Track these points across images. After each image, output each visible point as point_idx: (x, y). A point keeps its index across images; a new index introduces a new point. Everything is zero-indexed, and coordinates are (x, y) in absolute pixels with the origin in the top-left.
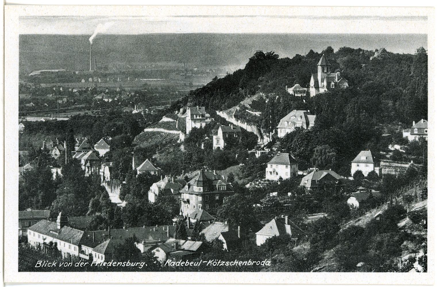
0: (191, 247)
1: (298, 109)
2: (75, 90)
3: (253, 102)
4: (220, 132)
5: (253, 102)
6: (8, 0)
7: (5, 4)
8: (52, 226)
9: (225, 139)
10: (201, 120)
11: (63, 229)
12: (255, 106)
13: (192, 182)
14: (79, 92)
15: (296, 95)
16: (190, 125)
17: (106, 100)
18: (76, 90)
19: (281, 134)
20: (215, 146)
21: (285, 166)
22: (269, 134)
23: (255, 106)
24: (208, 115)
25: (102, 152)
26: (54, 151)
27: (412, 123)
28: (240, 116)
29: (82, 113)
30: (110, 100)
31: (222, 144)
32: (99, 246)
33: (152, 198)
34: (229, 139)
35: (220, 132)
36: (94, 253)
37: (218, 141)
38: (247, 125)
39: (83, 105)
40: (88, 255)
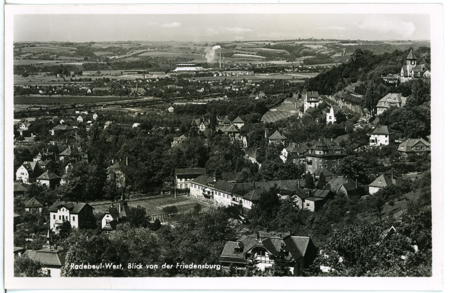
0: (321, 194)
1: (392, 92)
2: (209, 82)
3: (356, 87)
4: (332, 110)
5: (356, 87)
6: (8, 1)
7: (5, 3)
8: (209, 179)
9: (336, 116)
10: (315, 102)
11: (218, 182)
12: (358, 91)
13: (314, 147)
14: (213, 83)
15: (390, 82)
16: (307, 106)
17: (234, 89)
18: (210, 82)
19: (380, 112)
20: (328, 120)
21: (385, 136)
22: (370, 111)
23: (358, 91)
24: (320, 98)
25: (240, 126)
26: (201, 126)
27: (31, 117)
28: (348, 100)
29: (217, 99)
30: (237, 90)
31: (333, 120)
32: (247, 194)
33: (283, 159)
34: (339, 116)
35: (332, 110)
36: (243, 200)
37: (330, 118)
38: (352, 105)
39: (217, 94)
40: (238, 202)
